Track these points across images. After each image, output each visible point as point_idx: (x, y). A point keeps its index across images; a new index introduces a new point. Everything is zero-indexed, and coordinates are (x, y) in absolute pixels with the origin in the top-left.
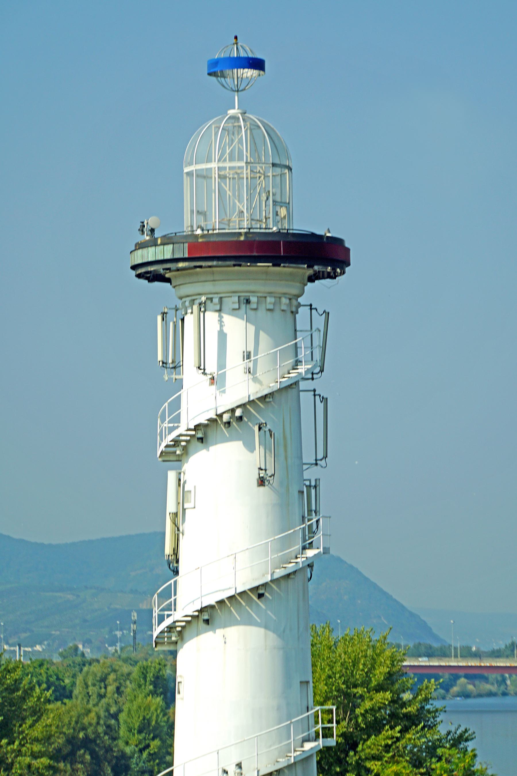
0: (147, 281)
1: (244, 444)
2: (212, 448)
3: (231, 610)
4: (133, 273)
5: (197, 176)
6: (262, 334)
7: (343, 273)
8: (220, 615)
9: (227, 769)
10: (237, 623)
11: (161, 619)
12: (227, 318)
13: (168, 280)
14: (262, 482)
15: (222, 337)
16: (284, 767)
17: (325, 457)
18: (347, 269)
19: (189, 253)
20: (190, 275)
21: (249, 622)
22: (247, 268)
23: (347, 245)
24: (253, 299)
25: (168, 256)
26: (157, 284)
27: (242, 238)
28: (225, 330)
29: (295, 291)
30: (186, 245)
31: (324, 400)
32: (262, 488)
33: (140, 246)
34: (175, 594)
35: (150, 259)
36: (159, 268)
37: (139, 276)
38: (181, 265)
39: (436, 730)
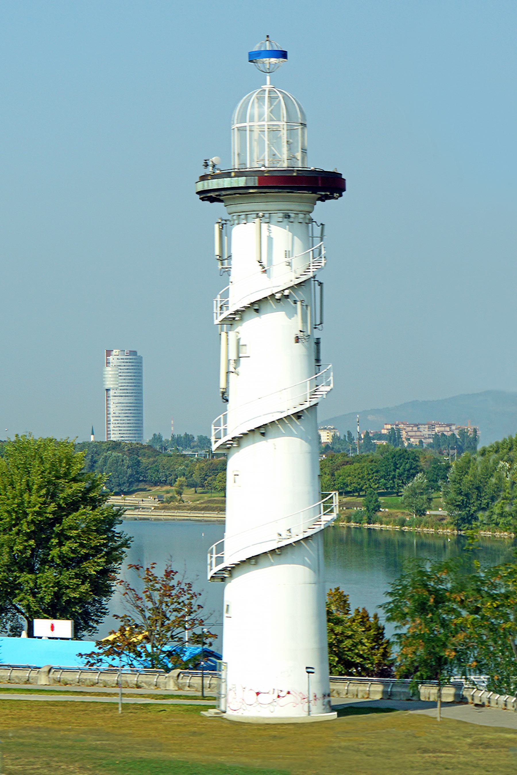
0: (209, 202)
1: (286, 314)
2: (262, 316)
3: (278, 427)
4: (198, 196)
5: (238, 130)
6: (295, 238)
7: (341, 196)
8: (271, 431)
9: (280, 533)
10: (284, 435)
11: (218, 438)
12: (273, 227)
13: (222, 201)
14: (297, 340)
15: (270, 239)
16: (301, 540)
17: (321, 323)
18: (344, 193)
19: (259, 184)
20: (254, 197)
21: (291, 434)
22: (273, 194)
23: (343, 177)
24: (292, 215)
25: (242, 184)
26: (216, 203)
27: (295, 174)
28: (272, 235)
29: (307, 209)
30: (256, 177)
31: (320, 284)
32: (297, 344)
33: (203, 178)
34: (225, 423)
35: (226, 186)
36: (213, 194)
37: (202, 199)
38: (251, 191)
39: (7, 715)
